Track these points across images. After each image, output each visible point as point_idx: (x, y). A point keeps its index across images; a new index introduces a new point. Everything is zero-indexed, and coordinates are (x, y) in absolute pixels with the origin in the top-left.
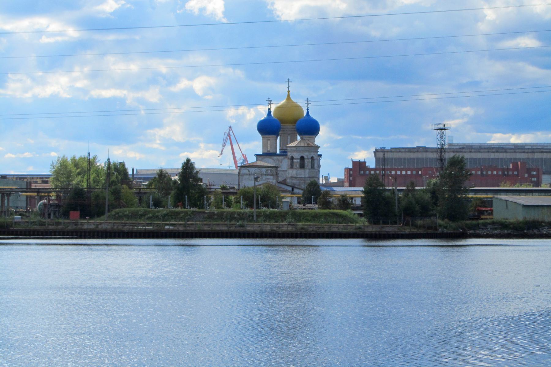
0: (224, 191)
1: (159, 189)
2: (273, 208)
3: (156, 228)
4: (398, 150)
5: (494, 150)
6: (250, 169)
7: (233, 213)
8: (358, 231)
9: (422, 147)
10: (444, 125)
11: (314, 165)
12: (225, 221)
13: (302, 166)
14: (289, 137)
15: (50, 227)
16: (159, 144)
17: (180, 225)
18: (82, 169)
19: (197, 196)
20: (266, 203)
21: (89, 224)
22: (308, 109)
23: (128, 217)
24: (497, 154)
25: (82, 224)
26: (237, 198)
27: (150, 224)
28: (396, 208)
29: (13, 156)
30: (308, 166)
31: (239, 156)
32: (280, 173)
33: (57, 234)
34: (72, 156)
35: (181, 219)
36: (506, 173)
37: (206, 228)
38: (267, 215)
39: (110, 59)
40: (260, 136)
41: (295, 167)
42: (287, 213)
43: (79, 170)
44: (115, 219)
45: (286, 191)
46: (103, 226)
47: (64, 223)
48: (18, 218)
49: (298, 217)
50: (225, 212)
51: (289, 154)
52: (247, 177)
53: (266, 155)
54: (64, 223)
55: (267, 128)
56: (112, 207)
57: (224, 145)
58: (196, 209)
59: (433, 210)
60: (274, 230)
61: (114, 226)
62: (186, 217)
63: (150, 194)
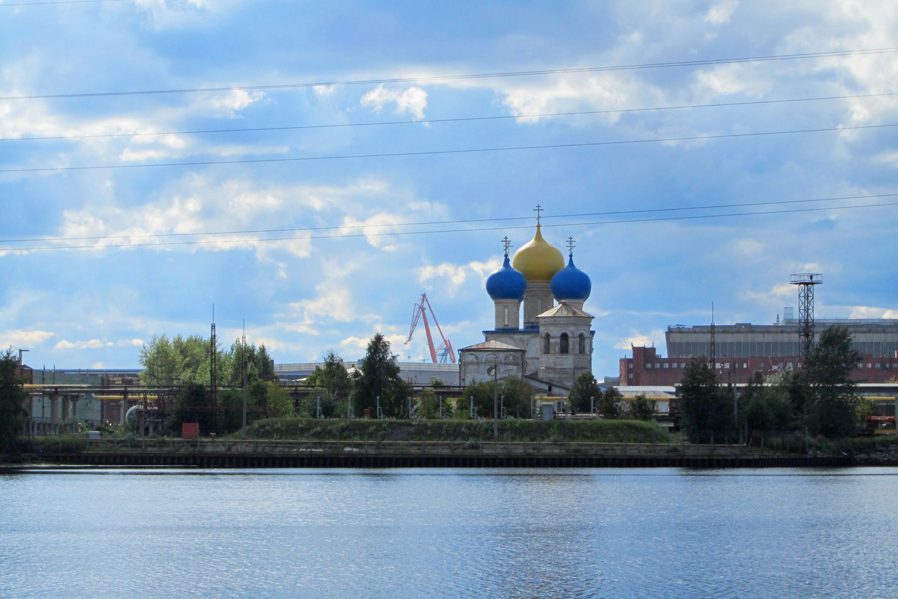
0: (439, 390)
1: (328, 387)
2: (524, 417)
3: (328, 451)
5: (864, 329)
7: (459, 426)
9: (746, 325)
10: (811, 277)
11: (584, 348)
12: (446, 439)
13: (564, 350)
14: (539, 302)
15: (149, 449)
17: (371, 445)
18: (193, 356)
19: (393, 398)
21: (214, 444)
22: (571, 256)
23: (280, 432)
24: (868, 335)
25: (203, 444)
26: (462, 401)
27: (319, 445)
28: (736, 413)
29: (70, 345)
30: (574, 349)
31: (438, 343)
32: (529, 361)
33: (155, 461)
34: (176, 337)
35: (371, 436)
36: (887, 365)
37: (413, 451)
39: (233, 186)
40: (490, 303)
42: (550, 425)
43: (187, 359)
44: (263, 435)
45: (539, 391)
47: (173, 442)
48: (95, 434)
49: (569, 431)
50: (444, 424)
51: (542, 330)
52: (475, 367)
53: (502, 331)
54: (174, 443)
55: (503, 288)
56: (253, 415)
57: (414, 325)
58: (394, 419)
59: (797, 419)
60: (530, 454)
61: (257, 447)
62: (380, 433)
63: (317, 394)
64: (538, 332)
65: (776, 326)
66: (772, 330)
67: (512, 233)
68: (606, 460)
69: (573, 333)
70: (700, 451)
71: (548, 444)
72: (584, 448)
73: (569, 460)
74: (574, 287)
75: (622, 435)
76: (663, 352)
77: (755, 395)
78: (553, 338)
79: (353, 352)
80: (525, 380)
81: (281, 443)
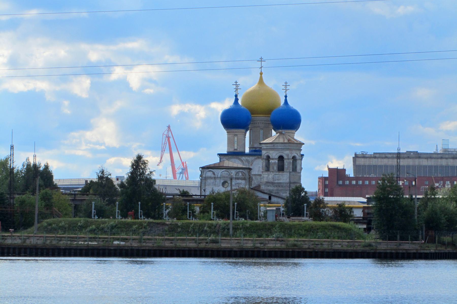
3: (101, 244)
4: (384, 156)
6: (215, 171)
7: (202, 225)
8: (367, 249)
9: (414, 152)
11: (296, 167)
12: (192, 235)
14: (262, 132)
16: (84, 150)
17: (134, 239)
20: (242, 213)
22: (286, 97)
23: (64, 229)
27: (94, 239)
28: (416, 217)
31: (178, 165)
32: (254, 177)
35: (134, 232)
37: (168, 244)
38: (247, 227)
40: (223, 132)
41: (271, 169)
42: (272, 225)
44: (50, 231)
46: (32, 240)
49: (288, 230)
50: (191, 223)
51: (264, 152)
52: (212, 181)
53: (232, 154)
55: (233, 121)
56: (43, 216)
57: (163, 151)
58: (151, 220)
61: (46, 240)
62: (141, 230)
64: (261, 155)
65: (435, 154)
66: (434, 156)
67: (241, 81)
68: (316, 253)
69: (288, 155)
70: (389, 246)
71: (272, 240)
72: (299, 243)
73: (288, 252)
74: (288, 121)
75: (329, 233)
76: (350, 172)
77: (429, 204)
78: (273, 159)
79: (119, 170)
80: (252, 191)
81: (64, 237)
